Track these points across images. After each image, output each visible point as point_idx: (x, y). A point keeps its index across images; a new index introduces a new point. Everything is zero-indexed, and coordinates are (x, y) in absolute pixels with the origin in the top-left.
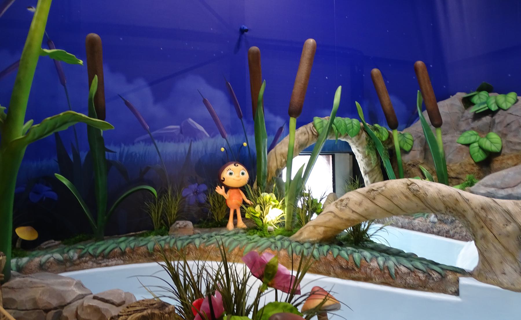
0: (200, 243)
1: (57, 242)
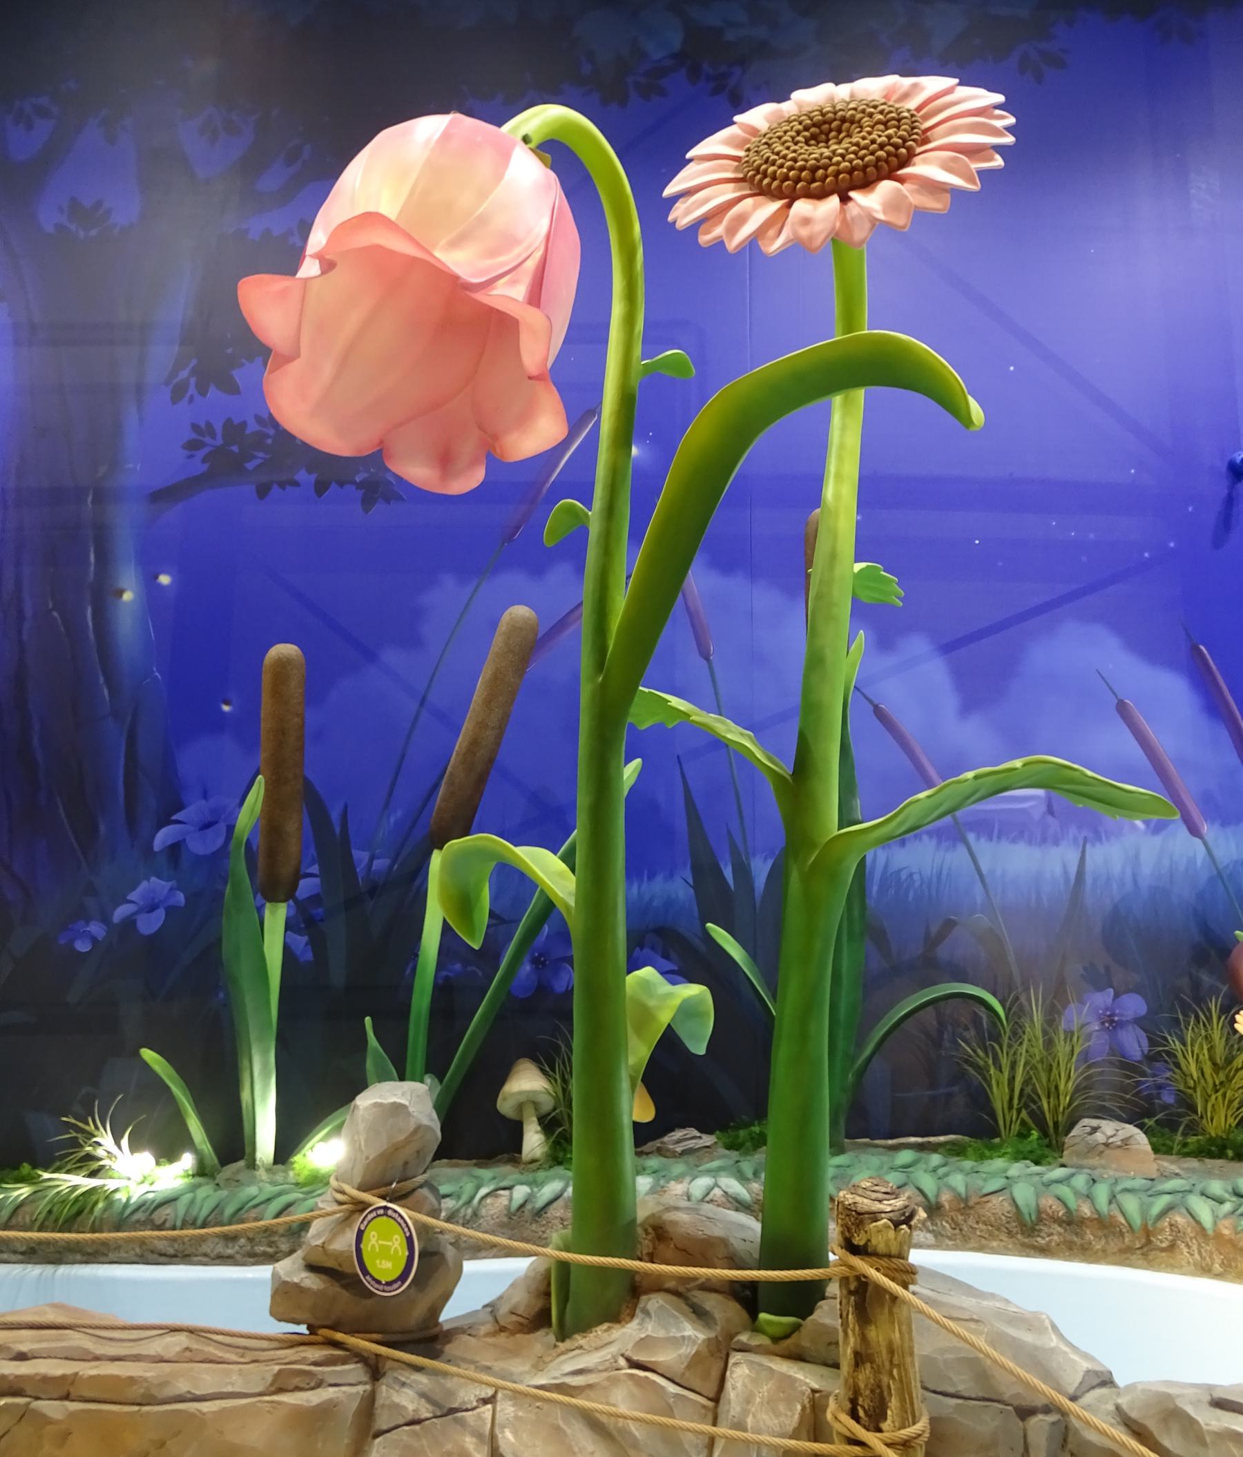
0: (1216, 1218)
1: (708, 1140)
